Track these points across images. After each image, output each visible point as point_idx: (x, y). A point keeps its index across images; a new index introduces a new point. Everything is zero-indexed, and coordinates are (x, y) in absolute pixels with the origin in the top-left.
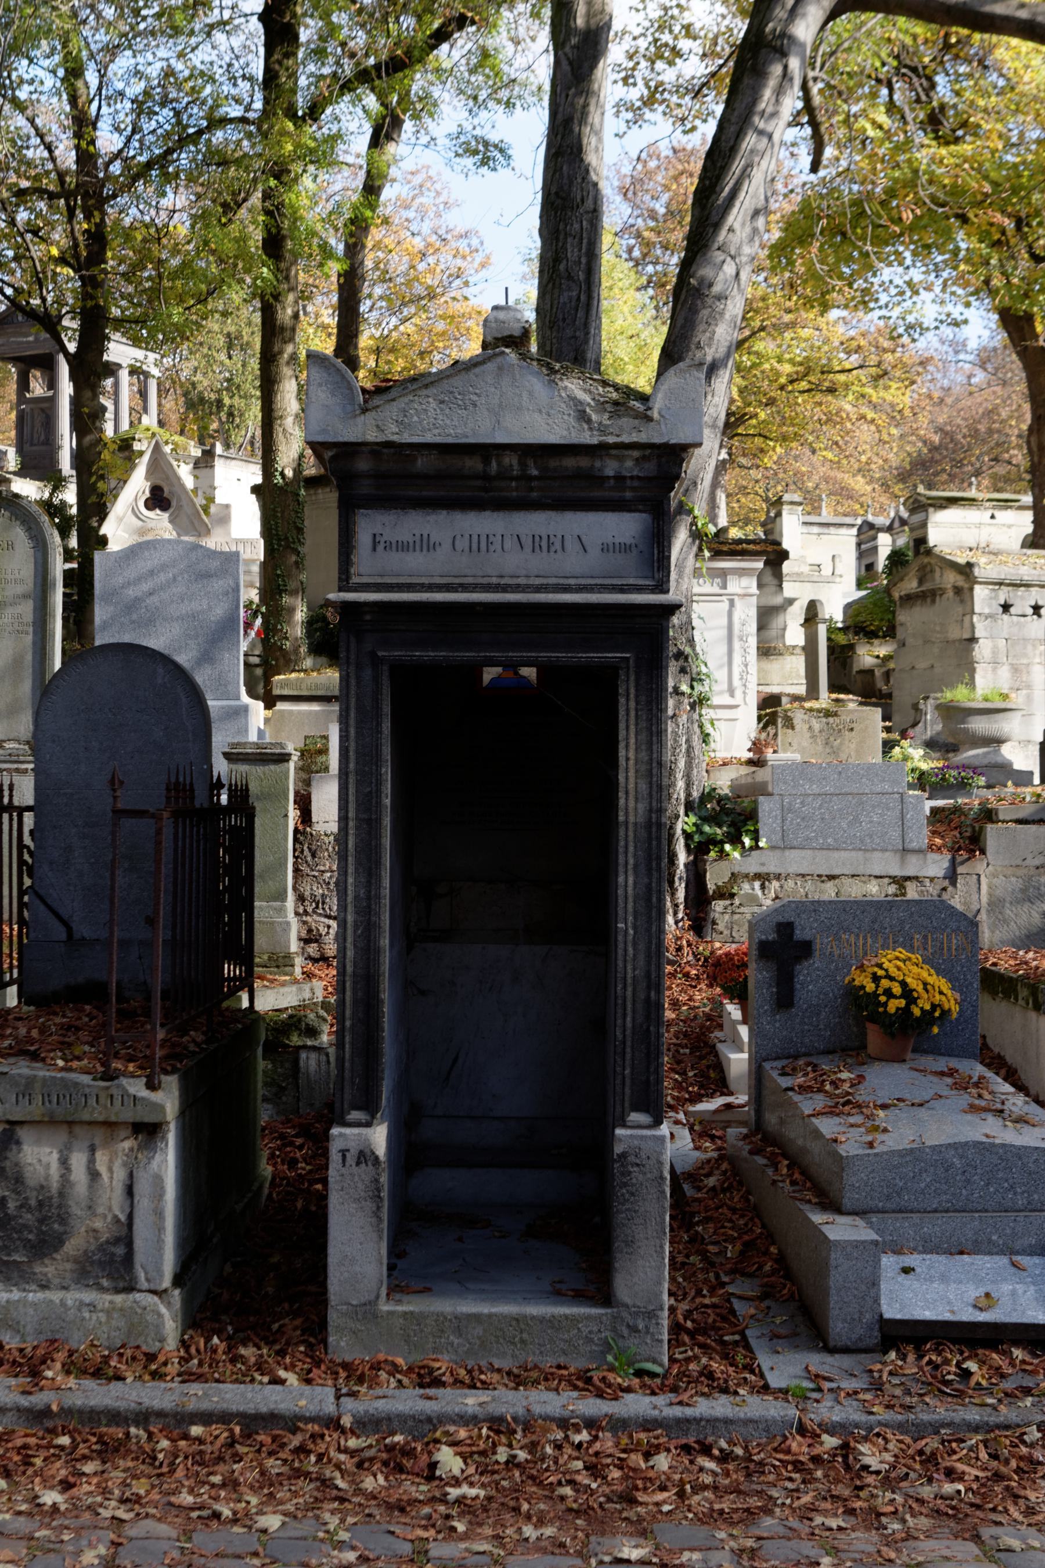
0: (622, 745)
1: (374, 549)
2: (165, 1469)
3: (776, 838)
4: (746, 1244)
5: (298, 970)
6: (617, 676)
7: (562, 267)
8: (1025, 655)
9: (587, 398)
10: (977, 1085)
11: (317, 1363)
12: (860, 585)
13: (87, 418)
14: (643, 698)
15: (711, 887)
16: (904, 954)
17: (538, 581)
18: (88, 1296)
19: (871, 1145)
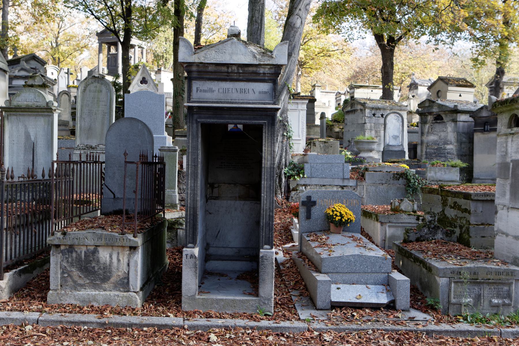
0: (264, 146)
1: (197, 92)
2: (136, 339)
3: (309, 175)
4: (296, 282)
5: (178, 208)
6: (262, 128)
7: (254, 19)
8: (379, 128)
9: (256, 51)
10: (359, 240)
11: (179, 311)
12: (336, 109)
13: (126, 60)
14: (270, 133)
15: (291, 188)
16: (341, 205)
17: (241, 101)
18: (117, 293)
19: (330, 255)
